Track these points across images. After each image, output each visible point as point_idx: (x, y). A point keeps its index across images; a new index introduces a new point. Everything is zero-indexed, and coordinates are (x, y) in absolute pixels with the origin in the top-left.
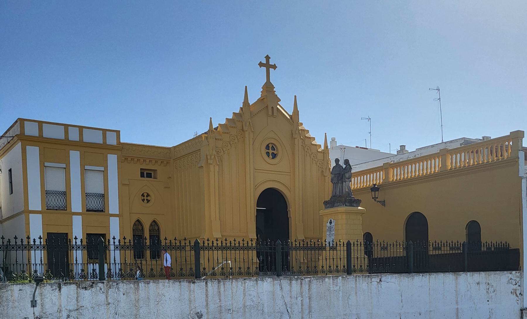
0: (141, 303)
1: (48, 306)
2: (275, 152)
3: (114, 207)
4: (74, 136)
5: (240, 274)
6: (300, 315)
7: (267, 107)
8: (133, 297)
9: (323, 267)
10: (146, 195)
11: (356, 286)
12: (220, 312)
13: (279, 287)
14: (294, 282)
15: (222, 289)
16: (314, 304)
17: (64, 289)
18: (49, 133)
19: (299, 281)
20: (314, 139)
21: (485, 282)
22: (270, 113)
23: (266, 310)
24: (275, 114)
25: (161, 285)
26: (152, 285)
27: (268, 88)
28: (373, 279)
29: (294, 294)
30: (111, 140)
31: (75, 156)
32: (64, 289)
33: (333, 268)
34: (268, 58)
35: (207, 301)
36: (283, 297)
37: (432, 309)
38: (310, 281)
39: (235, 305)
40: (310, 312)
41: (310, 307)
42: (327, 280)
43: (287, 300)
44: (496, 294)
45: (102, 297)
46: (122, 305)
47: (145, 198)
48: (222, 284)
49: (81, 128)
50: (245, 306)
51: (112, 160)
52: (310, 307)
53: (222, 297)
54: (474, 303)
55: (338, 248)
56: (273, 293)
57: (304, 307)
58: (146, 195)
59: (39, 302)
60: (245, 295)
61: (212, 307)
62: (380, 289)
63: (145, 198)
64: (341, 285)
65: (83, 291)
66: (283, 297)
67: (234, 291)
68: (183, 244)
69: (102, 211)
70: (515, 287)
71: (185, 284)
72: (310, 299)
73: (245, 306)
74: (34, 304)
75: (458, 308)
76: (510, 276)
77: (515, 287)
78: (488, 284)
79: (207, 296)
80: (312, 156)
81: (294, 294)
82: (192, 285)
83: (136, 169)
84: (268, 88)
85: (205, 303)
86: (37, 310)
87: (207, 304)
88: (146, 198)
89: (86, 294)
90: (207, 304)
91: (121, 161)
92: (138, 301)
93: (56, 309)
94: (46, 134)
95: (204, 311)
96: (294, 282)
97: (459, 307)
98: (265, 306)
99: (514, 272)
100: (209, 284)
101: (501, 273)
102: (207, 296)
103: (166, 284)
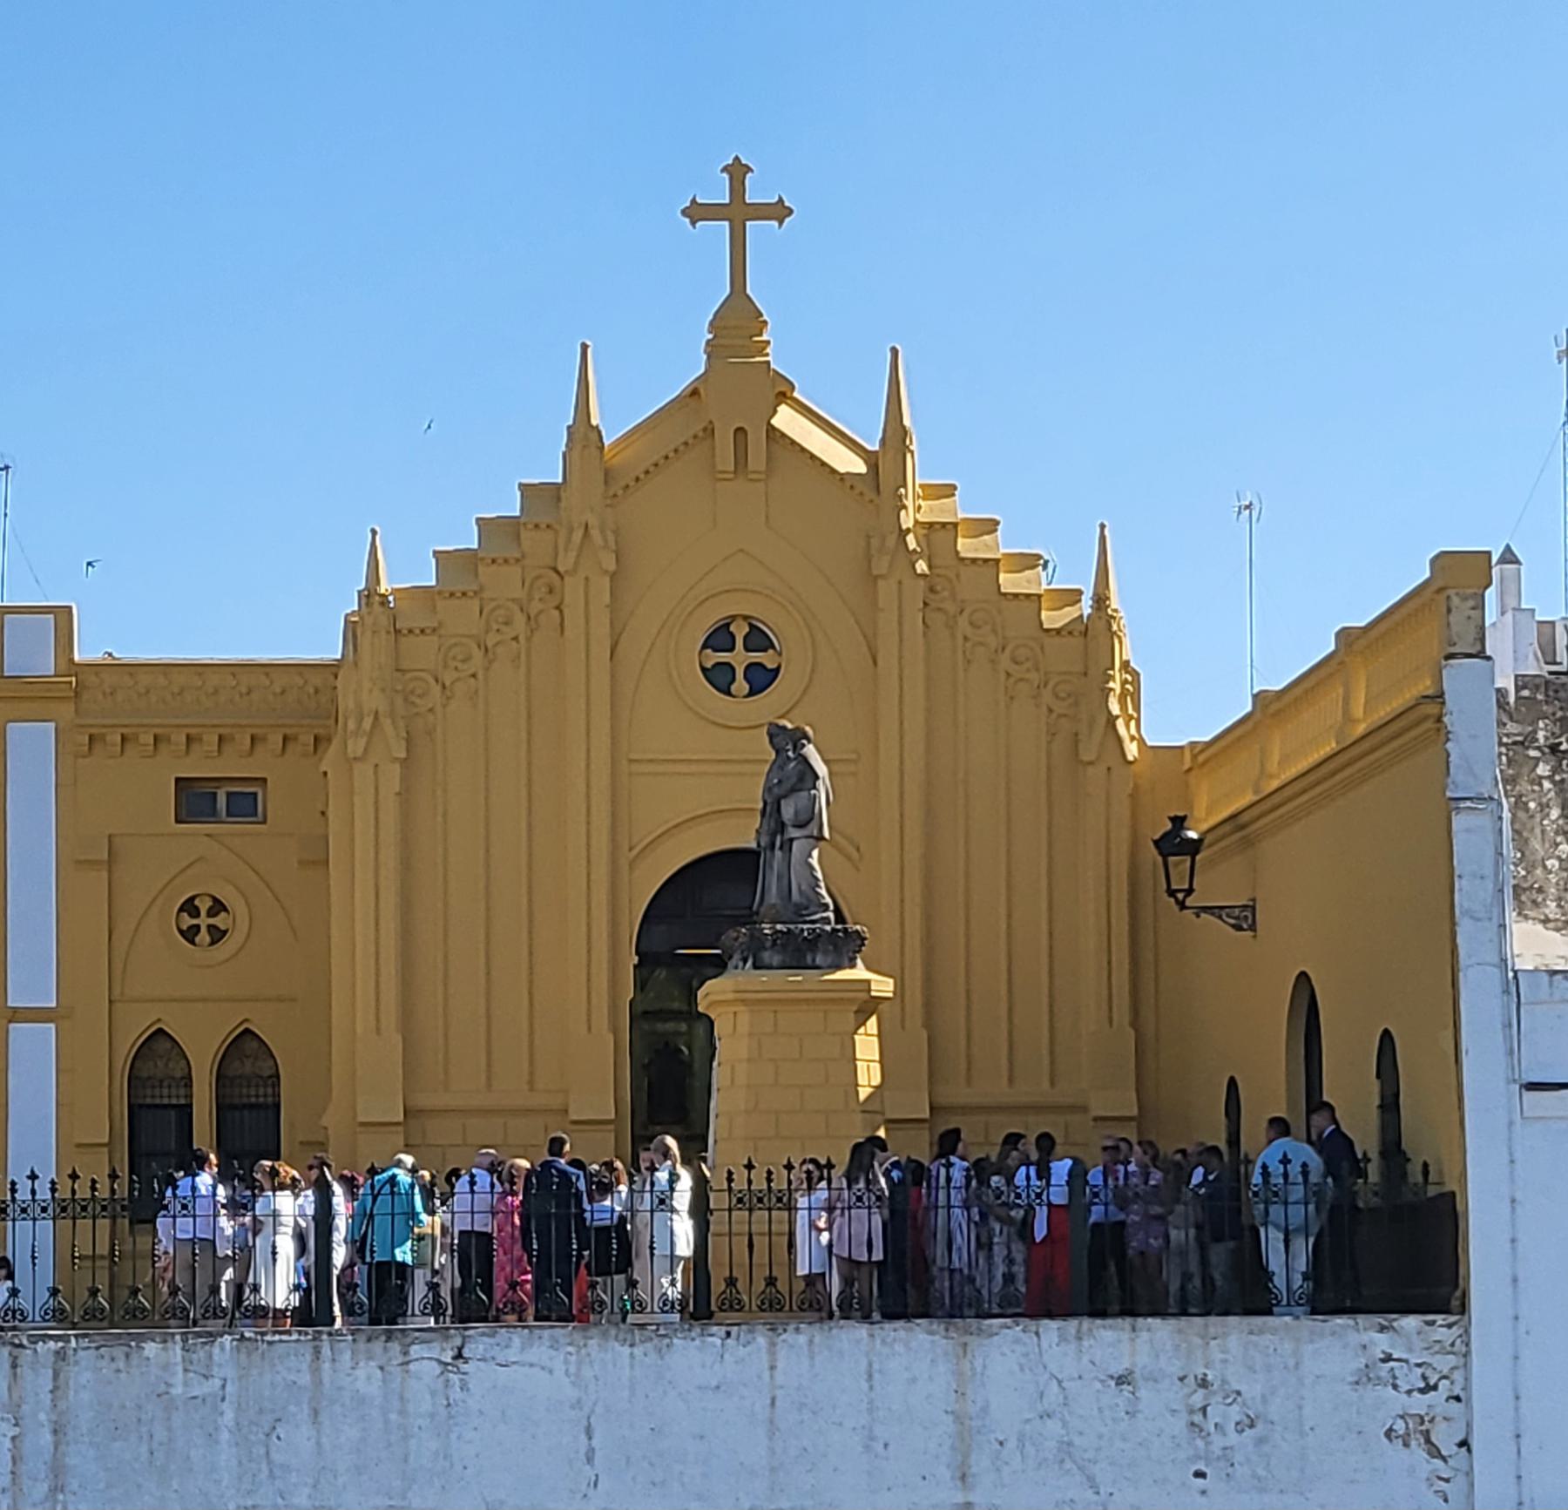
2: (767, 659)
7: (710, 431)
9: (731, 1282)
10: (204, 905)
11: (318, 1382)
16: (78, 1457)
24: (757, 459)
28: (416, 1350)
38: (60, 1355)
40: (57, 1489)
41: (57, 1471)
42: (151, 1348)
47: (203, 921)
52: (57, 1471)
58: (204, 905)
63: (203, 921)
64: (230, 1372)
70: (1419, 1404)
76: (1382, 1343)
77: (1419, 1404)
78: (1203, 1383)
99: (1411, 1322)
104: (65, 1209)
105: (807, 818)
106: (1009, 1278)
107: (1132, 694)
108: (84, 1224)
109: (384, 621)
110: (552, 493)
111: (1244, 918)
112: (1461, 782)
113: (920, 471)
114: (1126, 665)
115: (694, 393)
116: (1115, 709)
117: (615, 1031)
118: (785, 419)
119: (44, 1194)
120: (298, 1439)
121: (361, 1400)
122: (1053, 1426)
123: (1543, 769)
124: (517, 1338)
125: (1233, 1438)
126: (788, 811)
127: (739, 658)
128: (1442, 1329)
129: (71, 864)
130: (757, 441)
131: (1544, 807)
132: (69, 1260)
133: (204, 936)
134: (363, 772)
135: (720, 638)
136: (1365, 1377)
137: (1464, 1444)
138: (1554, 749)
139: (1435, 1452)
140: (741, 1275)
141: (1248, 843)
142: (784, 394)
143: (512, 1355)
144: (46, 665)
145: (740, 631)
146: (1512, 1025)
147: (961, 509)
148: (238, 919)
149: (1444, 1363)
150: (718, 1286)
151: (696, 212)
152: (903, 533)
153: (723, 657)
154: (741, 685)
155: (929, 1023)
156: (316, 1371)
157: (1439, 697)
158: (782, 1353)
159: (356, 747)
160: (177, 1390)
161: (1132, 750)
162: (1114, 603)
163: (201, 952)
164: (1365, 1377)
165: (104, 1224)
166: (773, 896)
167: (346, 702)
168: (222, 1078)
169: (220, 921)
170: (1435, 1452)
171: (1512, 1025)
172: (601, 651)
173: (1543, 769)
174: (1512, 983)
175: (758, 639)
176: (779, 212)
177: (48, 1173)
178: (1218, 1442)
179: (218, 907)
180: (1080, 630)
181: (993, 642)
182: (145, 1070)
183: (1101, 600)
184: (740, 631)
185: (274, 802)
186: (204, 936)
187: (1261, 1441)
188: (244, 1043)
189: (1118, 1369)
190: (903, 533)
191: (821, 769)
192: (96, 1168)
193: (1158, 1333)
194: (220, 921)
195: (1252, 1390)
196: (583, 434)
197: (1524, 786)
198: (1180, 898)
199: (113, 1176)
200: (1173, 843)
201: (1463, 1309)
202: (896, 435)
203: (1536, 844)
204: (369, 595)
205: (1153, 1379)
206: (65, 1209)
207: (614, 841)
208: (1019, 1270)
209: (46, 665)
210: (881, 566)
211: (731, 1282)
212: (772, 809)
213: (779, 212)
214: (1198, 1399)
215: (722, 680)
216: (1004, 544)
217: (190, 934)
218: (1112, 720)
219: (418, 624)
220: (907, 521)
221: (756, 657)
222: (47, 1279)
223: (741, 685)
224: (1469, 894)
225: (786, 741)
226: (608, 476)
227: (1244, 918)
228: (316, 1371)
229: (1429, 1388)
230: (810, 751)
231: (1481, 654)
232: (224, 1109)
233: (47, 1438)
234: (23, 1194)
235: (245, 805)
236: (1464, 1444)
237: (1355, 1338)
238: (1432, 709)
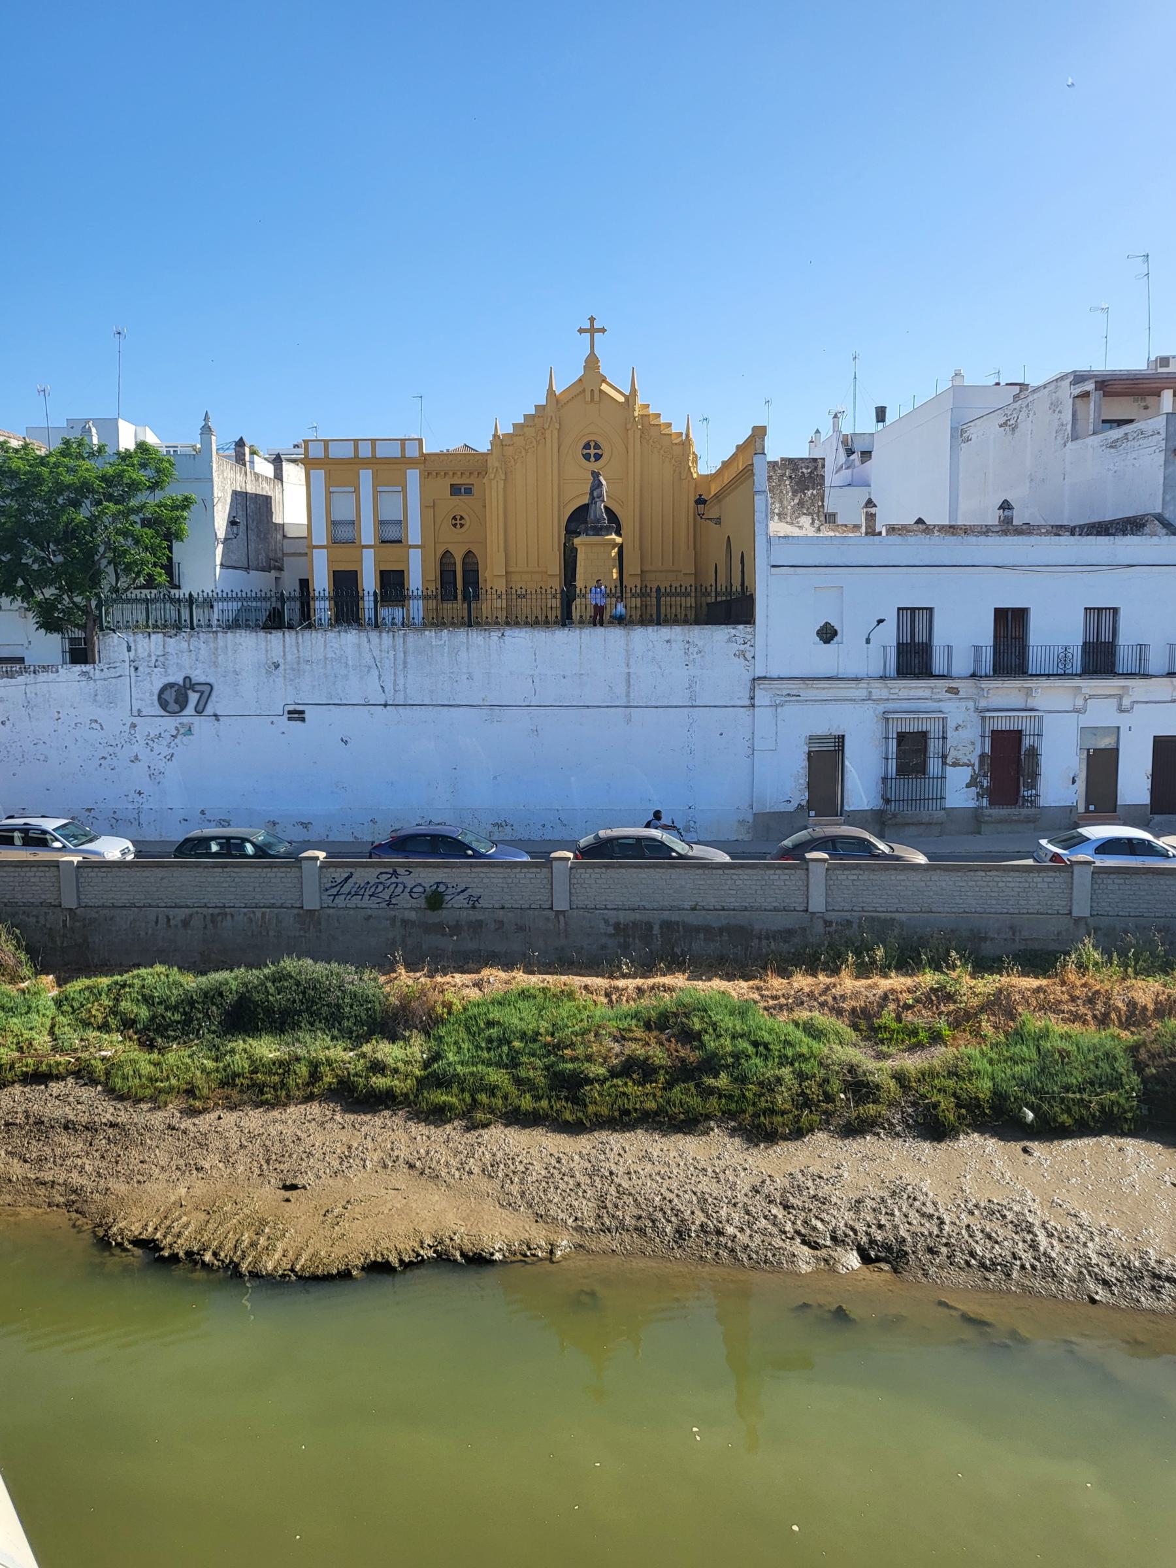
0: (219, 650)
1: (140, 650)
2: (599, 452)
3: (414, 536)
4: (365, 452)
5: (527, 624)
6: (393, 670)
7: (584, 390)
8: (212, 645)
9: (666, 616)
10: (458, 518)
11: (468, 642)
12: (299, 663)
13: (366, 639)
14: (384, 634)
15: (300, 640)
16: (410, 659)
17: (153, 637)
18: (335, 452)
19: (391, 633)
20: (669, 425)
21: (681, 638)
22: (588, 398)
23: (350, 663)
24: (596, 398)
25: (238, 635)
26: (230, 635)
27: (592, 362)
28: (492, 634)
29: (384, 647)
30: (412, 452)
31: (366, 476)
32: (153, 637)
33: (541, 618)
34: (592, 319)
35: (284, 651)
36: (371, 650)
37: (582, 672)
38: (405, 634)
39: (315, 656)
40: (405, 667)
41: (405, 662)
42: (427, 633)
43: (376, 653)
44: (703, 656)
45: (184, 645)
46: (202, 652)
47: (458, 522)
48: (300, 635)
49: (374, 441)
50: (326, 658)
51: (413, 476)
52: (405, 662)
53: (301, 649)
54: (660, 667)
55: (529, 596)
56: (359, 646)
57: (397, 662)
58: (458, 518)
59: (133, 648)
60: (325, 646)
61: (289, 657)
62: (502, 644)
63: (458, 522)
64: (446, 639)
65: (168, 639)
66: (371, 650)
67: (314, 642)
68: (268, 595)
69: (401, 542)
70: (742, 647)
71: (262, 634)
72: (405, 653)
73: (326, 658)
74: (129, 649)
75: (629, 674)
76: (733, 632)
77: (742, 647)
78: (688, 642)
79: (284, 647)
80: (662, 452)
81: (384, 647)
82: (269, 636)
83: (444, 485)
84: (592, 362)
85: (282, 654)
86: (132, 653)
87: (284, 655)
88: (457, 521)
89: (171, 642)
90: (284, 655)
91: (427, 475)
92: (216, 649)
93: (146, 654)
94: (333, 454)
95: (281, 661)
96: (384, 634)
97: (631, 671)
98: (349, 658)
99: (741, 627)
100: (287, 635)
101: (714, 627)
102: (284, 647)
103: (243, 634)
104: (425, 598)
105: (600, 496)
106: (557, 617)
107: (695, 461)
108: (430, 601)
109: (499, 443)
110: (543, 407)
111: (718, 521)
112: (757, 487)
113: (640, 401)
114: (694, 453)
115: (580, 380)
116: (690, 464)
117: (559, 550)
118: (604, 387)
119: (420, 593)
120: (463, 654)
121: (479, 646)
122: (650, 653)
123: (787, 482)
124: (517, 630)
125: (695, 656)
126: (595, 494)
127: (592, 452)
128: (749, 629)
129: (424, 507)
130: (597, 393)
131: (787, 493)
132: (426, 610)
133: (458, 526)
134: (494, 483)
135: (587, 446)
136: (729, 640)
137: (753, 657)
138: (791, 477)
139: (746, 659)
140: (490, 617)
141: (719, 501)
142: (604, 380)
143: (516, 635)
144: (416, 454)
145: (592, 444)
146: (769, 550)
147: (652, 411)
148: (467, 522)
149: (749, 637)
150: (663, 616)
151: (581, 331)
152: (635, 418)
153: (588, 451)
154: (592, 459)
155: (641, 549)
156: (468, 638)
157: (752, 465)
158: (583, 636)
159: (492, 476)
160: (434, 643)
161: (695, 476)
162: (691, 436)
163: (458, 530)
164: (729, 640)
165: (327, 603)
166: (592, 517)
167: (489, 465)
168: (464, 563)
169: (462, 522)
170: (746, 659)
171: (769, 550)
172: (555, 450)
173: (787, 482)
174: (769, 540)
175: (597, 446)
176: (603, 330)
177: (421, 589)
178: (692, 657)
179: (462, 518)
180: (683, 444)
181: (659, 447)
182: (444, 561)
183: (687, 435)
184: (592, 444)
185: (475, 490)
186: (458, 526)
187: (703, 656)
188: (469, 553)
189: (667, 638)
190: (635, 418)
191: (604, 482)
192: (432, 587)
193: (678, 629)
194: (462, 522)
195: (700, 644)
196: (551, 392)
197: (782, 487)
198: (701, 515)
199: (616, 587)
200: (700, 501)
201: (754, 623)
202: (634, 391)
203: (785, 502)
204: (495, 436)
205: (675, 641)
206: (425, 598)
207: (559, 501)
208: (559, 615)
209: (416, 454)
210: (629, 426)
211: (666, 616)
212: (591, 493)
213: (603, 330)
214: (687, 646)
215: (587, 456)
216: (663, 420)
217: (455, 525)
218: (689, 468)
219: (509, 443)
220: (636, 414)
221: (596, 451)
222: (421, 615)
223: (592, 459)
224: (759, 516)
225: (595, 475)
226: (557, 401)
227: (718, 521)
228: (468, 638)
229: (745, 643)
230: (601, 478)
231: (764, 453)
232: (464, 571)
233: (402, 655)
234: (415, 593)
235: (469, 491)
236: (753, 657)
237: (726, 631)
238: (750, 468)
